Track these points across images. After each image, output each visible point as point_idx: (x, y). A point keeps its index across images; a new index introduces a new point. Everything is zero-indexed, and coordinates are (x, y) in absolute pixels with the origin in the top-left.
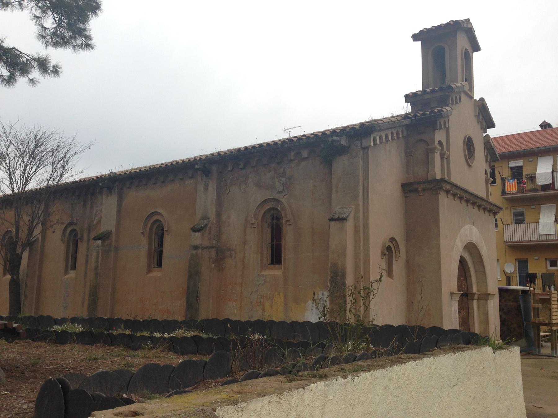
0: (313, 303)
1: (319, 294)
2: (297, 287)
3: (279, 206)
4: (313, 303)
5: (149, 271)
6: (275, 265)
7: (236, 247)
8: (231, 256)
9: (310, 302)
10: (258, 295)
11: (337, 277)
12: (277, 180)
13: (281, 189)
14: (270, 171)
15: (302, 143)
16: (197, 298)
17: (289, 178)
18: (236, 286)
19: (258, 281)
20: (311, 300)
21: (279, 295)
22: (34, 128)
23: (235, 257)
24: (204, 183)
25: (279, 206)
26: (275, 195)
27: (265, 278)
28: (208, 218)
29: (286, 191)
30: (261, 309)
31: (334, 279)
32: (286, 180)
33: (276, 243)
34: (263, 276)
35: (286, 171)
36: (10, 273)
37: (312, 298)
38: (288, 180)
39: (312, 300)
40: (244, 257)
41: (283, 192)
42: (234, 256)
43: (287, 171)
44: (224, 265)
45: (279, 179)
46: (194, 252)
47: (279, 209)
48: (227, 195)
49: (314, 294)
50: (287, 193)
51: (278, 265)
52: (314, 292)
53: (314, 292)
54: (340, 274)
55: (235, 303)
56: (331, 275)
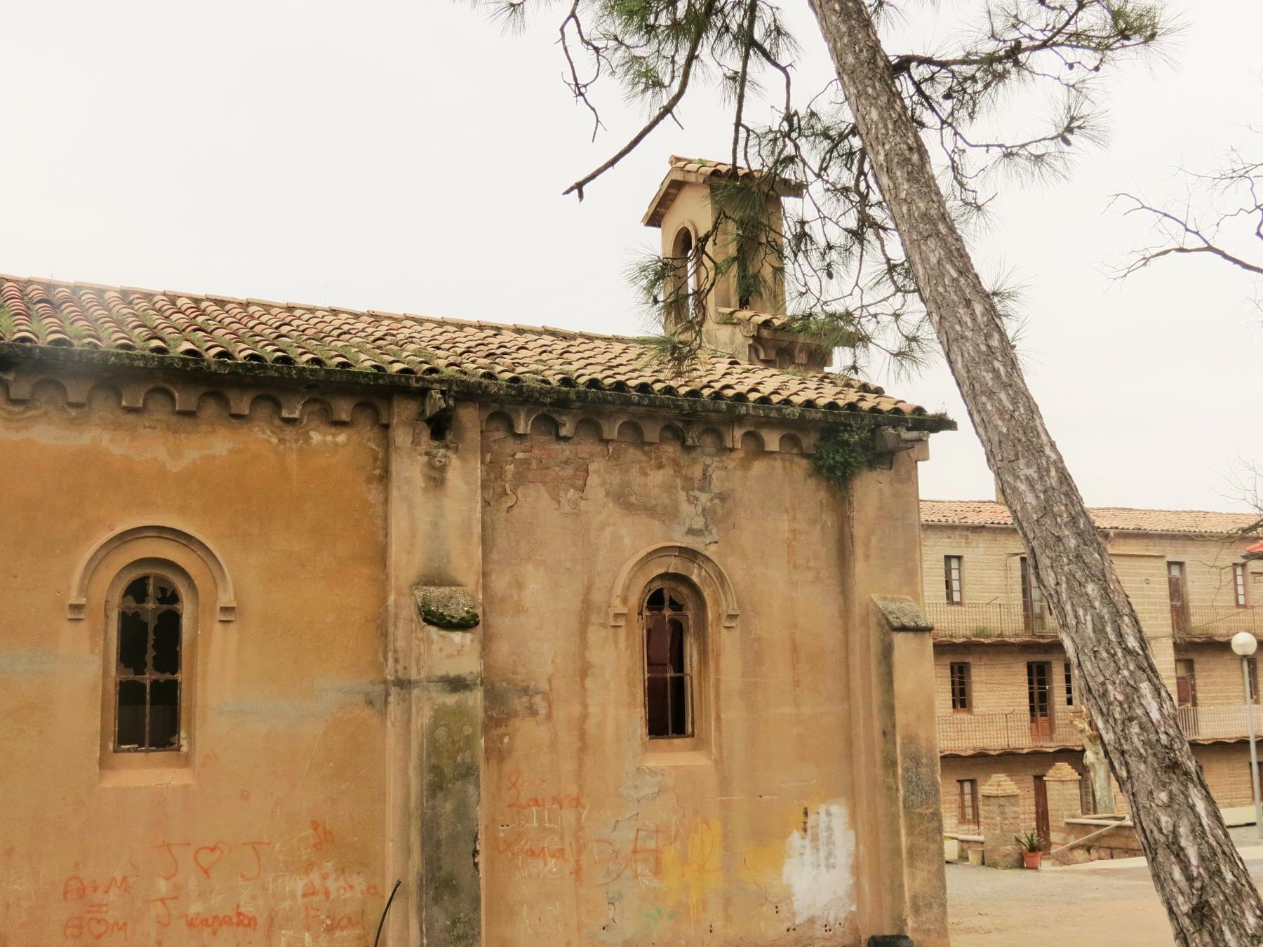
0: (803, 838)
1: (818, 813)
2: (759, 798)
3: (696, 571)
4: (803, 838)
5: (104, 764)
6: (673, 738)
7: (550, 682)
8: (532, 711)
9: (796, 836)
10: (638, 830)
11: (919, 770)
12: (682, 495)
13: (699, 523)
14: (660, 466)
15: (789, 415)
16: (474, 856)
17: (723, 497)
18: (556, 806)
19: (636, 787)
20: (798, 829)
21: (708, 824)
22: (993, 96)
23: (549, 717)
24: (426, 458)
25: (696, 571)
26: (681, 539)
27: (659, 778)
28: (452, 583)
29: (714, 531)
30: (650, 871)
31: (913, 773)
32: (712, 500)
33: (673, 674)
34: (652, 772)
35: (710, 476)
36: (1040, 810)
37: (801, 825)
38: (717, 501)
39: (801, 829)
40: (584, 717)
41: (706, 533)
42: (543, 712)
43: (713, 476)
44: (506, 740)
45: (691, 493)
46: (451, 700)
47: (695, 578)
48: (508, 512)
49: (806, 814)
50: (716, 538)
51: (179, 730)
52: (806, 809)
53: (806, 809)
54: (924, 760)
55: (554, 861)
56: (906, 765)
